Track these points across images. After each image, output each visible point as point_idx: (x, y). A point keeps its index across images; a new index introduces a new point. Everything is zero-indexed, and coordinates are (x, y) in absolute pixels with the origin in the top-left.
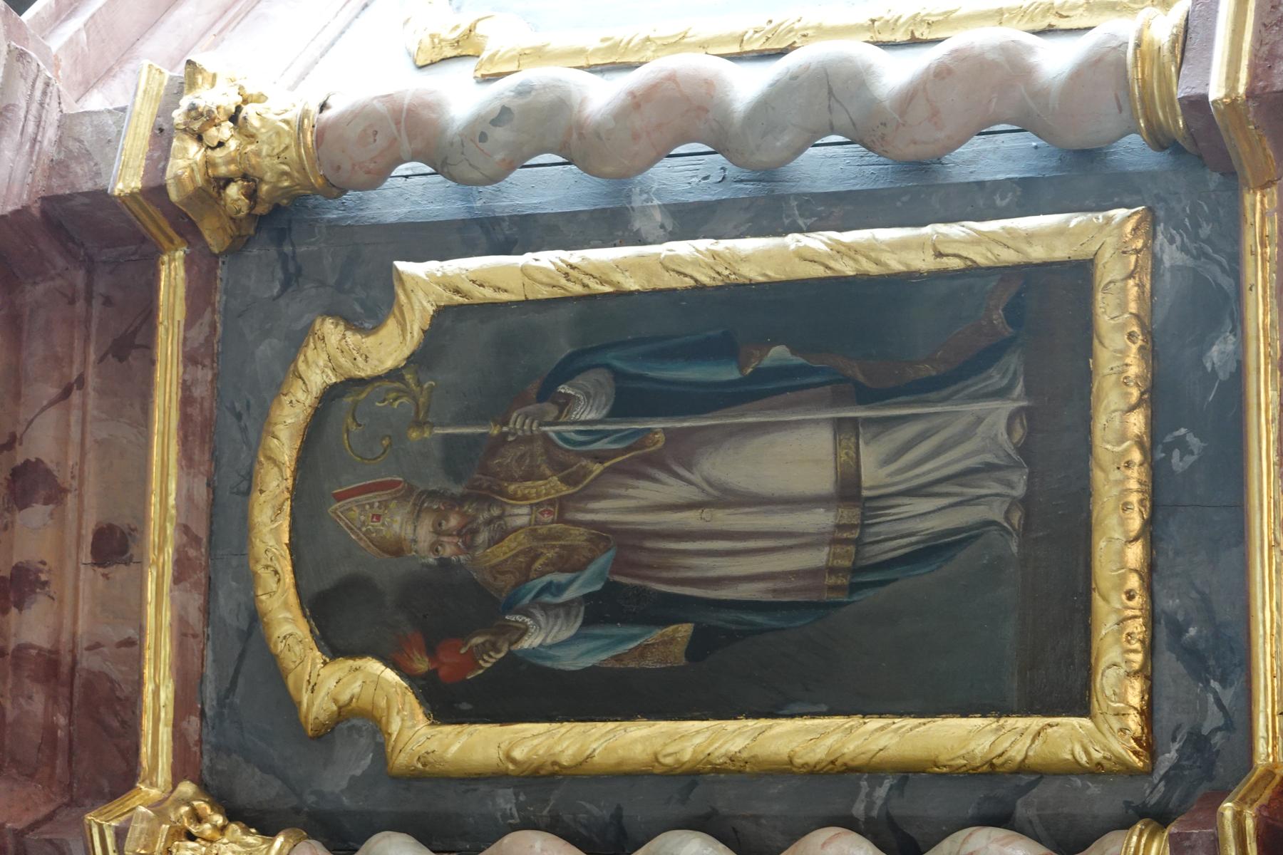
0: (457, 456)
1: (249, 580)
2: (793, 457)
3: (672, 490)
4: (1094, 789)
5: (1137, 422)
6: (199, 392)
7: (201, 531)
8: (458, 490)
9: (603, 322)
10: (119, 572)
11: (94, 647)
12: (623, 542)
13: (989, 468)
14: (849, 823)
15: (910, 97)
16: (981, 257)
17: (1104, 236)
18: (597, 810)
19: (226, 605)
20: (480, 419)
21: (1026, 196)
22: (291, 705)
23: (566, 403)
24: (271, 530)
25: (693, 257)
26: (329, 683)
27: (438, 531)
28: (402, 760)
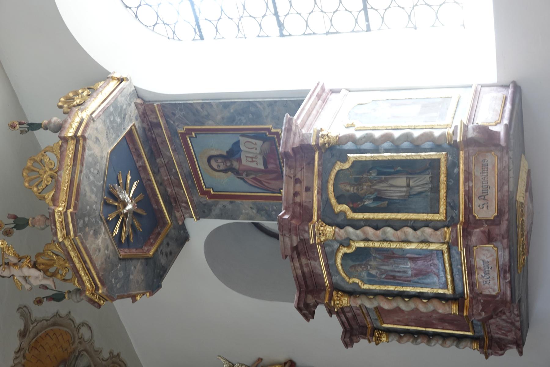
0: (356, 180)
1: (328, 194)
2: (402, 181)
3: (385, 185)
4: (439, 223)
5: (445, 179)
6: (320, 170)
7: (321, 187)
8: (356, 184)
9: (376, 163)
10: (309, 193)
11: (305, 202)
12: (379, 191)
13: (426, 184)
14: (408, 226)
15: (418, 138)
16: (426, 157)
17: (441, 155)
18: (375, 224)
19: (324, 197)
20: (360, 175)
21: (431, 150)
22: (334, 210)
23: (371, 173)
24: (331, 188)
25: (387, 155)
26: (339, 208)
27: (354, 189)
28: (349, 217)
